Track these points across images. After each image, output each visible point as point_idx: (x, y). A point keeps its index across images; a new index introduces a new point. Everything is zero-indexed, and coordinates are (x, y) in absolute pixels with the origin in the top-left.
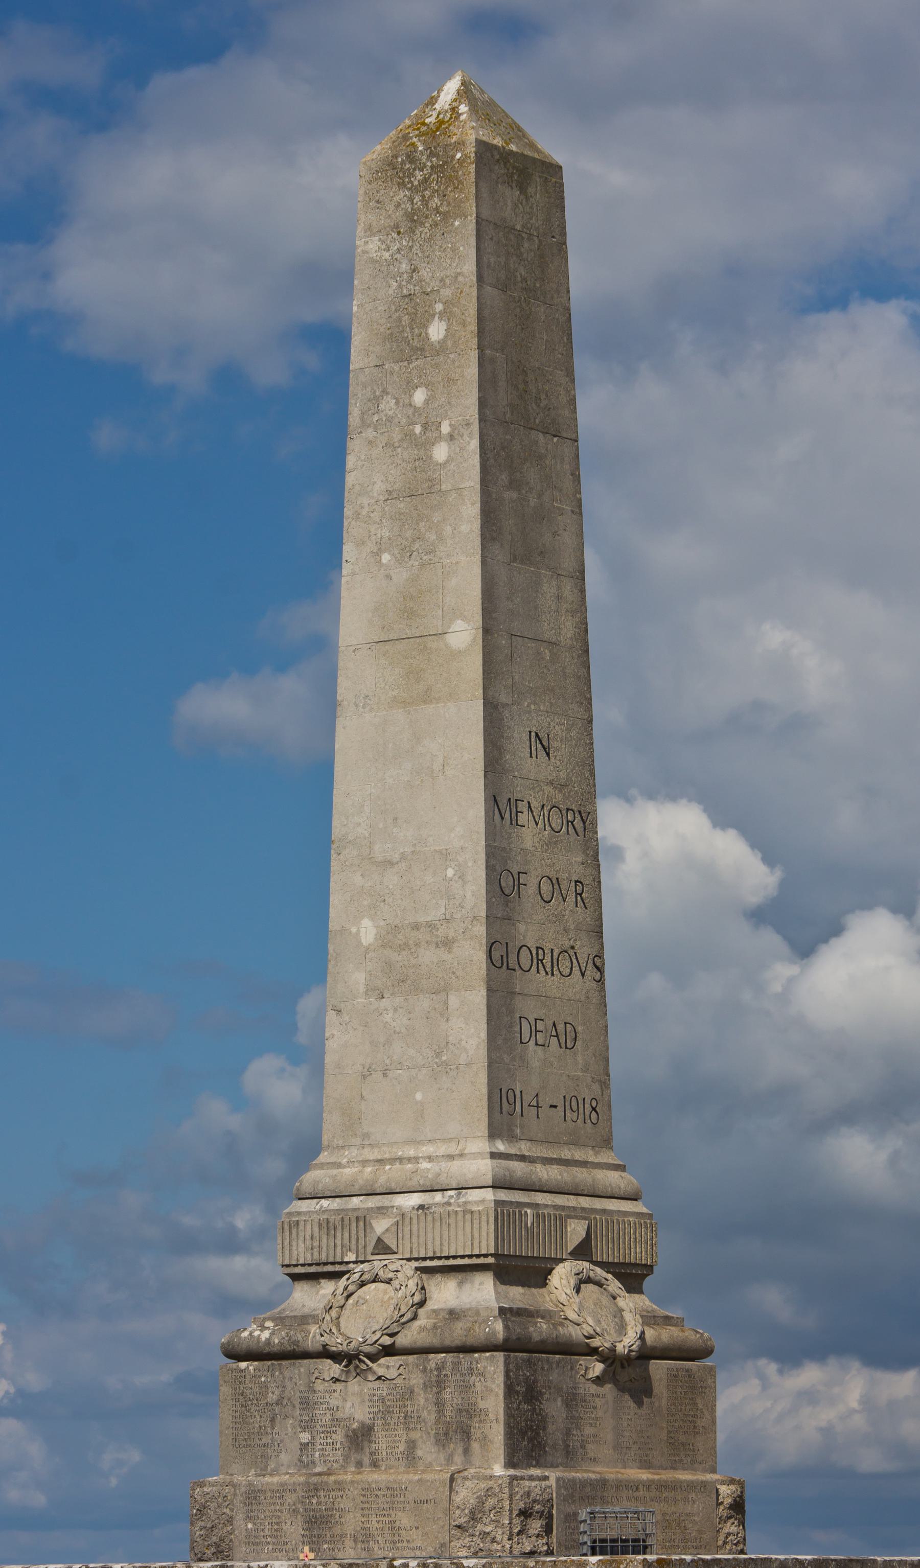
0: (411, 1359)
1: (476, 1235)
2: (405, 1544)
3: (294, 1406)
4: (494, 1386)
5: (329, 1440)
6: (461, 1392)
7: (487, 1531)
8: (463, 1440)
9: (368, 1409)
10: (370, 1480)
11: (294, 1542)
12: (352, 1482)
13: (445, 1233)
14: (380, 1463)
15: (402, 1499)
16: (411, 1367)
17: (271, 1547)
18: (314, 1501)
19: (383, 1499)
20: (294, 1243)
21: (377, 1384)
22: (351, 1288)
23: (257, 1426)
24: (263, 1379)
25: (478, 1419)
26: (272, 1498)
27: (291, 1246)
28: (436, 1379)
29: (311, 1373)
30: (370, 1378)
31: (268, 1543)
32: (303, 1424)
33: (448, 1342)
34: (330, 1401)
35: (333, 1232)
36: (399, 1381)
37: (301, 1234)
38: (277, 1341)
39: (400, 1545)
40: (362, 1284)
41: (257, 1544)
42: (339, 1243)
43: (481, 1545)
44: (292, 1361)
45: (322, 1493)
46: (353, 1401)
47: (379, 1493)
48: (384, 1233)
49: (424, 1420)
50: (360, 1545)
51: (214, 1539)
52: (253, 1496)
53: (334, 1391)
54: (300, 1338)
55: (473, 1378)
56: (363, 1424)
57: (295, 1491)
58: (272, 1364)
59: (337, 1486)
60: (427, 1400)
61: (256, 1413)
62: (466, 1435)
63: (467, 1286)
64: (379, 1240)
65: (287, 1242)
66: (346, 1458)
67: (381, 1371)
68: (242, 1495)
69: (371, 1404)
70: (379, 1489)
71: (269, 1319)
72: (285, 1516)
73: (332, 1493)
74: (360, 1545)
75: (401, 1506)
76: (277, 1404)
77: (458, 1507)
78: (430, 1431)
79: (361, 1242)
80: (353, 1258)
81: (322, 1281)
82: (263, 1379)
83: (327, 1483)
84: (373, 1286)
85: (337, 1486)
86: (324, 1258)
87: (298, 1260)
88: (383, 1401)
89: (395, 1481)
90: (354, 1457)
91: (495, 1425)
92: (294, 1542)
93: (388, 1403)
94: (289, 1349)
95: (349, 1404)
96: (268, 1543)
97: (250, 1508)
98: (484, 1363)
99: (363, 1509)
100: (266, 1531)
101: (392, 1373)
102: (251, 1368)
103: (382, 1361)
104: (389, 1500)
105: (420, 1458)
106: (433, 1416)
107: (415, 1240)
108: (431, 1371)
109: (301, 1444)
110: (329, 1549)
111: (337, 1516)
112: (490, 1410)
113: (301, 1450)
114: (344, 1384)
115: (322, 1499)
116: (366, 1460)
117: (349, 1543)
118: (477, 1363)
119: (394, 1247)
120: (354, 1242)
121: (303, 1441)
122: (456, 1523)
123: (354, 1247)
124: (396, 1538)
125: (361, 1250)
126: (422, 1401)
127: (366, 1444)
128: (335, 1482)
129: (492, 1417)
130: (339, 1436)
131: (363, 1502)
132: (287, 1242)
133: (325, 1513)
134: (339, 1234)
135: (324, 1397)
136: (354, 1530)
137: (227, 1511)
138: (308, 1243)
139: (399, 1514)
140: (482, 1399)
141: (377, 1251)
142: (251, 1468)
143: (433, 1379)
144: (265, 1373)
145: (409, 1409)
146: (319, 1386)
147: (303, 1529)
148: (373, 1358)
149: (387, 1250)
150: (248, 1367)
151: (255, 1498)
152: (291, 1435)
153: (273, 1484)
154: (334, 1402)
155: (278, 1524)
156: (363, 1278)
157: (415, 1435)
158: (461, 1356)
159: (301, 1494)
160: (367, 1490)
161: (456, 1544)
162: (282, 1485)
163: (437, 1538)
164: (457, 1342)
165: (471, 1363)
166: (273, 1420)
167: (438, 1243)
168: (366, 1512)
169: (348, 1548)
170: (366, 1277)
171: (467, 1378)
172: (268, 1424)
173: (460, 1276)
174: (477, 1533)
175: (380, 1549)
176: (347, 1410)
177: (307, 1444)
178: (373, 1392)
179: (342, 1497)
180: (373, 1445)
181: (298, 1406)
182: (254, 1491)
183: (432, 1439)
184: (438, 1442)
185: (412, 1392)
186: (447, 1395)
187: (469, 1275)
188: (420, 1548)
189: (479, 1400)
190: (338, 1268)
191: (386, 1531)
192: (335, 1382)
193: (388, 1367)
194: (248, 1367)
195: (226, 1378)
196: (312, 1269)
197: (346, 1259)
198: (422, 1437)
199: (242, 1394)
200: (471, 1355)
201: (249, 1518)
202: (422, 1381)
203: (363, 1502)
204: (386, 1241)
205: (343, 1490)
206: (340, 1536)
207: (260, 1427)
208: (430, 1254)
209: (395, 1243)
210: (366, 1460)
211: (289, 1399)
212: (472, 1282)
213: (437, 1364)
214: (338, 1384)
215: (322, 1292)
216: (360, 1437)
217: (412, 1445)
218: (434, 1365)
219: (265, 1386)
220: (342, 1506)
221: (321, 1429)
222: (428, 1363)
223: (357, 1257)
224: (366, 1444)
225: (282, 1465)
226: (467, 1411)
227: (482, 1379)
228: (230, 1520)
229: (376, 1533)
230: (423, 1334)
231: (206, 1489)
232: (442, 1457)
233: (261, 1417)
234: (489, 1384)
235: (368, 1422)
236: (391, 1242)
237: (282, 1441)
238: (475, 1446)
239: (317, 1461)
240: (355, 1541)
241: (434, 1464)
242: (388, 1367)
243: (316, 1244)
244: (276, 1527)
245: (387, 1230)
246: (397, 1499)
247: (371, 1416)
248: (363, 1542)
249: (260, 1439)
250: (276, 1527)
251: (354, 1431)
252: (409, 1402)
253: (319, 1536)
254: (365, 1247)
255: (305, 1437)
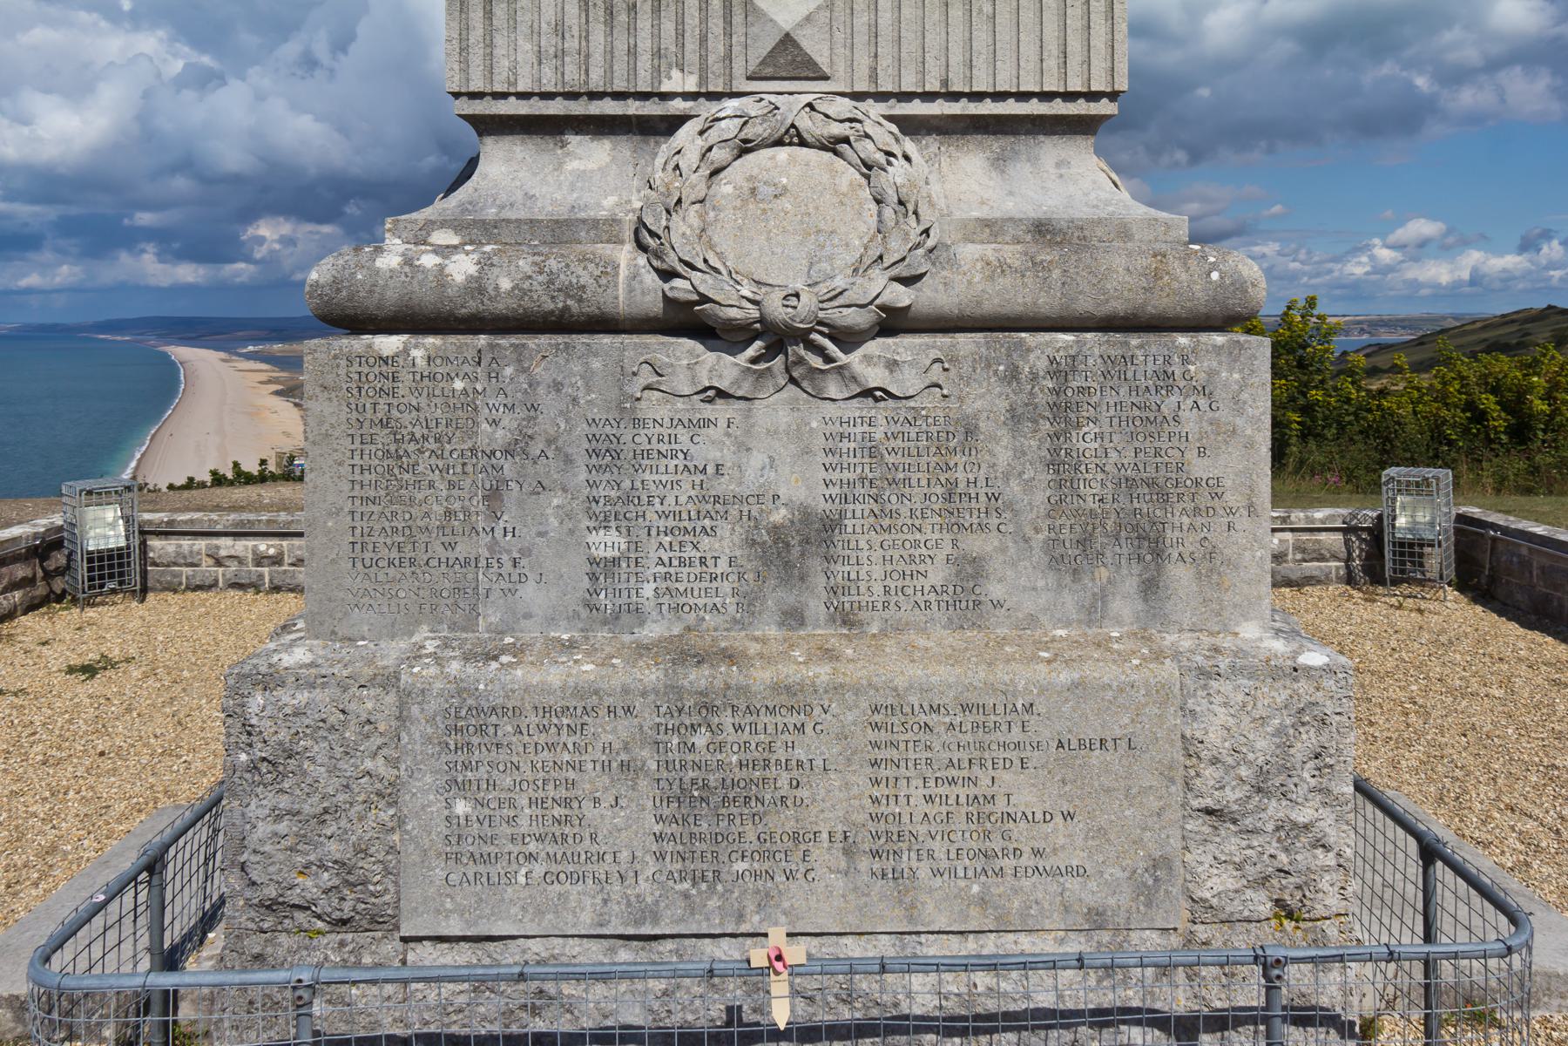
0: (966, 342)
1: (1075, 45)
2: (1027, 860)
3: (568, 460)
4: (1239, 422)
5: (689, 552)
6: (1133, 436)
7: (1301, 820)
8: (1140, 559)
9: (822, 474)
10: (900, 682)
11: (624, 855)
12: (837, 689)
13: (982, 38)
14: (863, 615)
15: (1016, 734)
16: (966, 369)
17: (539, 869)
18: (701, 739)
19: (948, 737)
20: (499, 40)
21: (855, 409)
22: (719, 155)
23: (438, 509)
24: (459, 385)
25: (1190, 506)
26: (544, 729)
27: (490, 45)
28: (1052, 399)
29: (625, 375)
30: (833, 389)
31: (530, 857)
32: (597, 509)
33: (1085, 304)
34: (693, 449)
35: (623, 18)
36: (929, 401)
37: (524, 18)
38: (506, 284)
39: (1008, 863)
40: (745, 148)
41: (486, 859)
42: (645, 44)
43: (1283, 858)
44: (561, 339)
45: (727, 719)
46: (779, 448)
47: (933, 719)
48: (800, 25)
49: (1010, 506)
50: (864, 864)
51: (334, 849)
52: (470, 724)
53: (707, 423)
54: (585, 279)
55: (1174, 399)
56: (806, 514)
57: (628, 710)
58: (492, 346)
59: (783, 699)
60: (1020, 453)
61: (436, 476)
62: (1150, 545)
63: (1020, 170)
64: (787, 41)
65: (477, 34)
66: (749, 603)
67: (875, 376)
68: (431, 720)
69: (829, 460)
70: (935, 709)
71: (443, 224)
72: (591, 780)
73: (765, 718)
74: (864, 864)
75: (1014, 755)
76: (508, 452)
77: (1215, 761)
78: (1029, 532)
79: (717, 47)
80: (691, 85)
81: (574, 140)
82: (459, 385)
83: (744, 690)
84: (782, 153)
85: (783, 699)
86: (596, 81)
87: (874, 76)
88: (873, 452)
89: (991, 688)
90: (776, 597)
91: (1242, 522)
92: (624, 855)
93: (890, 459)
94: (549, 306)
95: (757, 459)
96: (530, 857)
97: (461, 757)
98: (1210, 362)
99: (875, 763)
100: (524, 822)
101: (908, 382)
102: (418, 354)
103: (874, 347)
104: (969, 737)
105: (998, 605)
106: (1040, 497)
107: (885, 49)
108: (1034, 377)
109: (593, 561)
110: (756, 875)
111: (783, 781)
112: (1228, 483)
113: (593, 577)
114: (742, 404)
115: (729, 735)
116: (816, 607)
117: (824, 856)
118: (1185, 361)
119: (822, 60)
120: (691, 45)
121: (600, 553)
122: (1209, 802)
123: (691, 55)
124: (996, 844)
125: (715, 66)
126: (1004, 457)
127: (815, 564)
128: (776, 688)
129: (1231, 499)
130: (725, 543)
131: (876, 745)
132: (477, 34)
133: (738, 774)
134: (644, 23)
135: (673, 439)
136: (845, 821)
137: (379, 766)
138: (549, 42)
139: (1005, 777)
140: (1202, 452)
141: (769, 71)
142: (418, 623)
143: (1042, 399)
144: (467, 368)
145: (960, 475)
146: (654, 408)
147: (660, 819)
148: (848, 338)
149: (809, 71)
150: (406, 351)
151: (481, 730)
152: (555, 535)
153: (545, 689)
154: (706, 450)
155: (567, 803)
156: (749, 132)
157: (974, 544)
158: (1134, 340)
159: (650, 719)
160: (888, 712)
161: (1200, 858)
162: (578, 692)
163: (1138, 842)
164: (1118, 306)
165: (1168, 360)
166: (494, 496)
167: (956, 58)
168: (883, 773)
169: (821, 871)
170: (755, 131)
171: (1154, 398)
172: (477, 504)
173: (996, 144)
174: (1270, 827)
175: (937, 873)
176: (750, 475)
177: (615, 561)
178: (837, 428)
179: (800, 729)
180: (840, 568)
181: (581, 460)
182: (479, 710)
183: (1038, 555)
184: (1056, 561)
185: (970, 432)
186: (1085, 441)
187: (1023, 144)
188: (1080, 872)
189: (1192, 455)
190: (652, 108)
191: (959, 823)
192: (710, 401)
193: (892, 365)
194: (406, 351)
195: (329, 379)
196: (556, 108)
197: (666, 87)
198: (1003, 550)
199: (384, 424)
200: (1166, 338)
201: (457, 786)
202: (1003, 405)
203: (876, 745)
204: (806, 44)
205: (807, 709)
206: (795, 837)
207: (449, 513)
208: (933, 85)
209: (827, 53)
210: (816, 607)
211: (549, 442)
212: (1034, 160)
213: (1052, 361)
214: (720, 404)
215: (572, 165)
216: (795, 548)
217: (970, 571)
218: (1042, 364)
219: (469, 402)
220: (800, 753)
221: (662, 523)
222: (1024, 357)
223: (703, 79)
224: (815, 564)
225: (528, 616)
226: (1151, 483)
227: (1202, 402)
228: (390, 794)
229: (922, 830)
230: (1005, 282)
231: (284, 696)
232: (1069, 602)
233: (451, 485)
234: (1224, 414)
235: (822, 506)
236: (815, 47)
237: (526, 552)
238: (1179, 575)
239: (649, 606)
240: (847, 852)
241: (1044, 619)
242: (892, 365)
243: (572, 44)
244: (558, 811)
245: (808, 19)
246: (999, 736)
247: (834, 491)
248: (876, 854)
249: (452, 546)
250: (558, 811)
251: (775, 529)
252: (960, 459)
253: (716, 838)
254: (728, 57)
255: (607, 542)
